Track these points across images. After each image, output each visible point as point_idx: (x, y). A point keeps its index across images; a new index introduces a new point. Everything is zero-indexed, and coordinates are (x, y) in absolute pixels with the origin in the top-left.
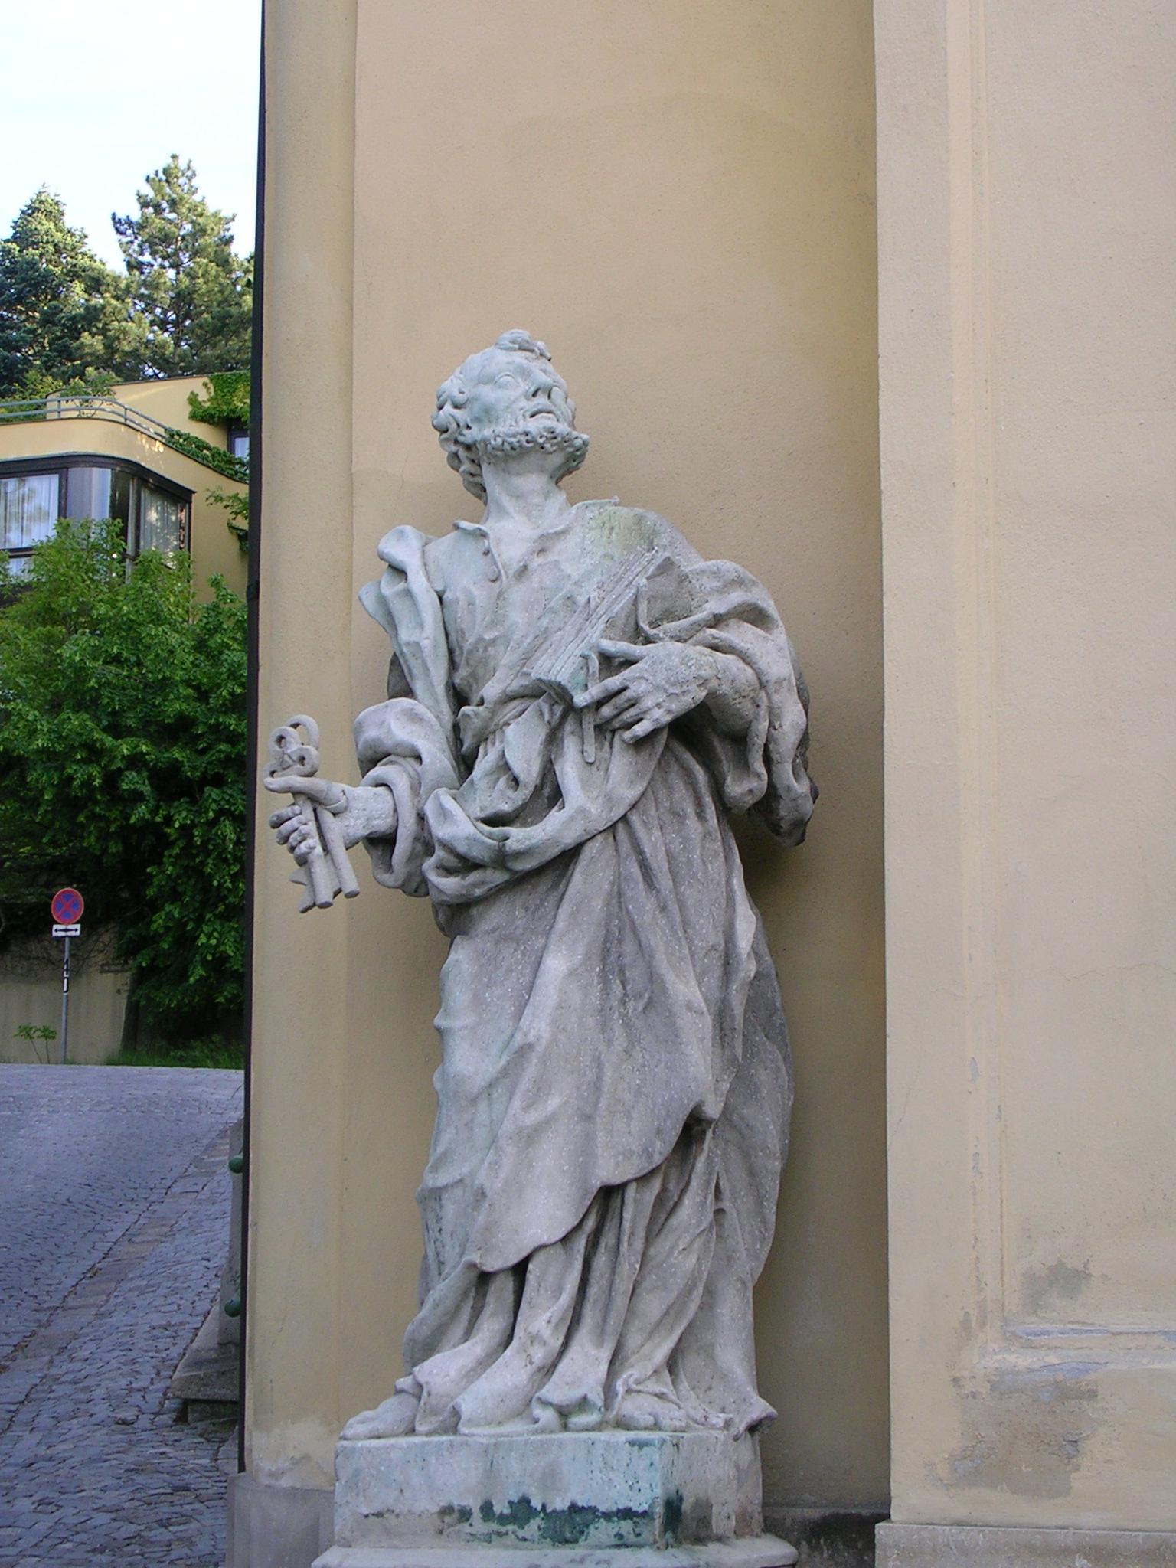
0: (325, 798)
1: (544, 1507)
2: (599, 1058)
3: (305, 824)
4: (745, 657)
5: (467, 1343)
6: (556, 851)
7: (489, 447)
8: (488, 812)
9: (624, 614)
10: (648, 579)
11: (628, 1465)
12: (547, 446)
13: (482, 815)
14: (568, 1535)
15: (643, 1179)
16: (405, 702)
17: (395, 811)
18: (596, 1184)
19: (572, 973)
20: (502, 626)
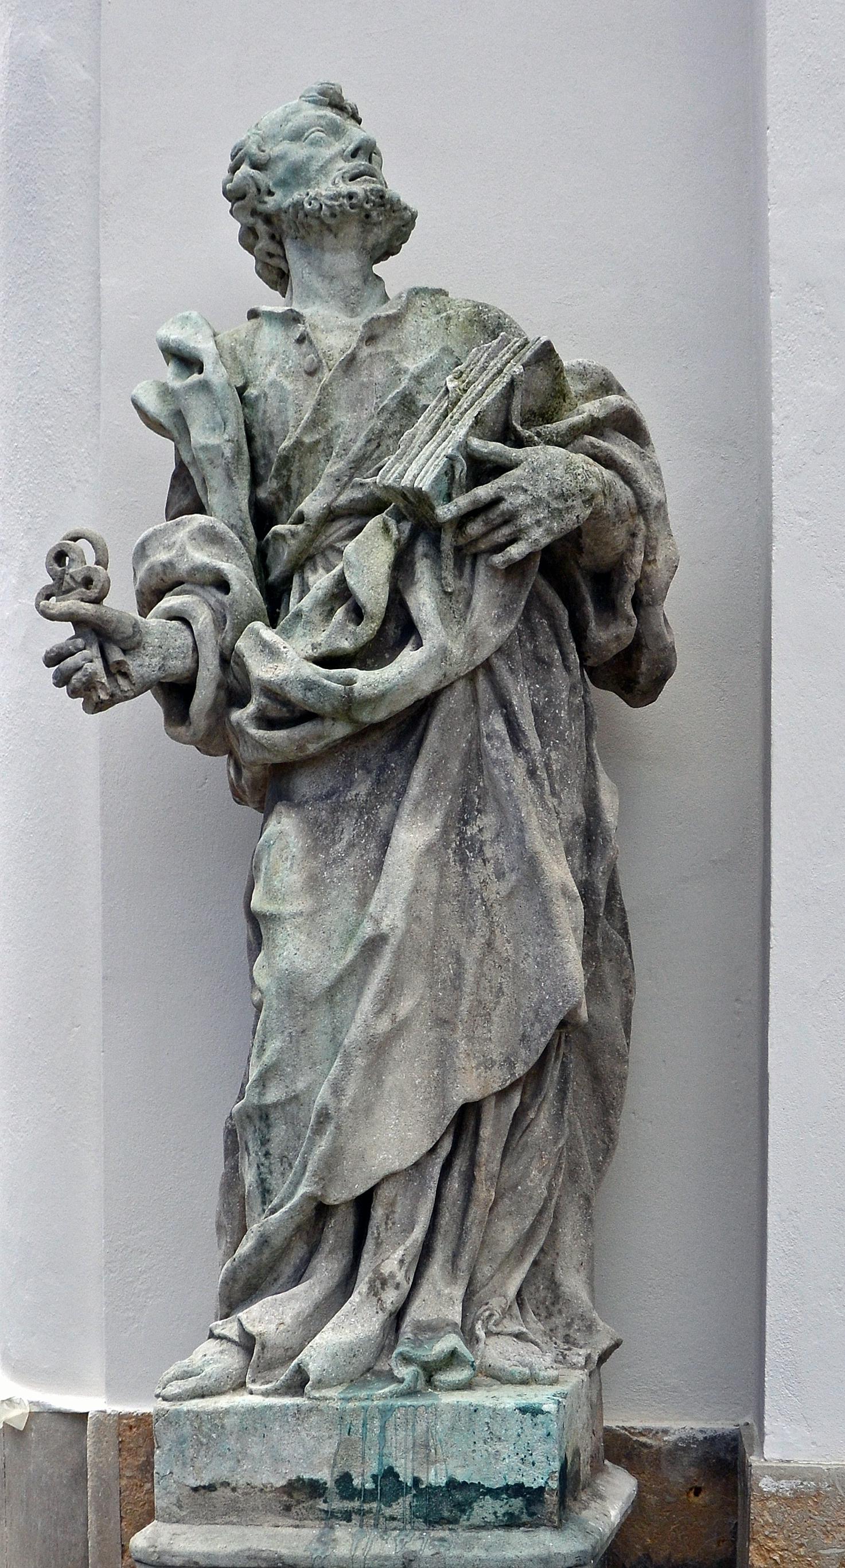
0: (114, 631)
1: (416, 1481)
2: (457, 953)
3: (91, 661)
4: (626, 475)
5: (301, 1287)
6: (408, 700)
7: (301, 215)
8: (323, 650)
9: (493, 408)
10: (524, 365)
11: (519, 1435)
12: (374, 214)
13: (316, 653)
14: (446, 1514)
15: (502, 1095)
16: (199, 519)
17: (195, 649)
18: (457, 1100)
19: (429, 850)
20: (324, 428)
